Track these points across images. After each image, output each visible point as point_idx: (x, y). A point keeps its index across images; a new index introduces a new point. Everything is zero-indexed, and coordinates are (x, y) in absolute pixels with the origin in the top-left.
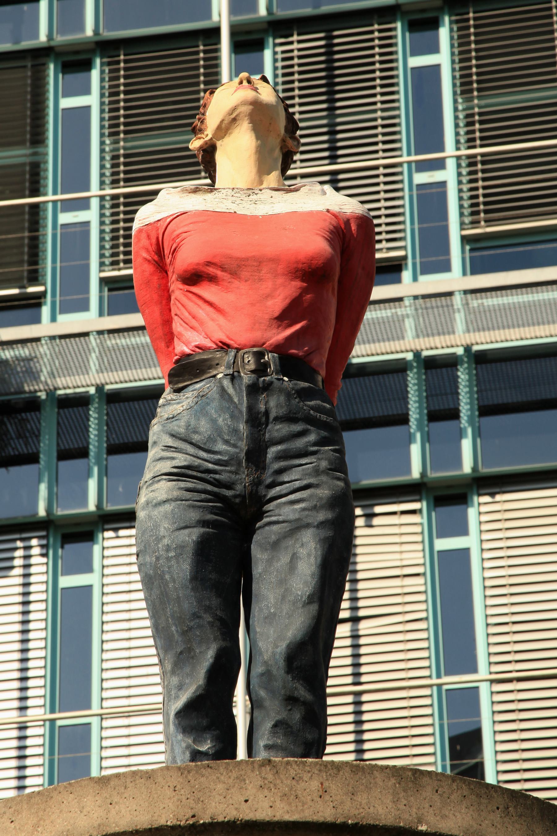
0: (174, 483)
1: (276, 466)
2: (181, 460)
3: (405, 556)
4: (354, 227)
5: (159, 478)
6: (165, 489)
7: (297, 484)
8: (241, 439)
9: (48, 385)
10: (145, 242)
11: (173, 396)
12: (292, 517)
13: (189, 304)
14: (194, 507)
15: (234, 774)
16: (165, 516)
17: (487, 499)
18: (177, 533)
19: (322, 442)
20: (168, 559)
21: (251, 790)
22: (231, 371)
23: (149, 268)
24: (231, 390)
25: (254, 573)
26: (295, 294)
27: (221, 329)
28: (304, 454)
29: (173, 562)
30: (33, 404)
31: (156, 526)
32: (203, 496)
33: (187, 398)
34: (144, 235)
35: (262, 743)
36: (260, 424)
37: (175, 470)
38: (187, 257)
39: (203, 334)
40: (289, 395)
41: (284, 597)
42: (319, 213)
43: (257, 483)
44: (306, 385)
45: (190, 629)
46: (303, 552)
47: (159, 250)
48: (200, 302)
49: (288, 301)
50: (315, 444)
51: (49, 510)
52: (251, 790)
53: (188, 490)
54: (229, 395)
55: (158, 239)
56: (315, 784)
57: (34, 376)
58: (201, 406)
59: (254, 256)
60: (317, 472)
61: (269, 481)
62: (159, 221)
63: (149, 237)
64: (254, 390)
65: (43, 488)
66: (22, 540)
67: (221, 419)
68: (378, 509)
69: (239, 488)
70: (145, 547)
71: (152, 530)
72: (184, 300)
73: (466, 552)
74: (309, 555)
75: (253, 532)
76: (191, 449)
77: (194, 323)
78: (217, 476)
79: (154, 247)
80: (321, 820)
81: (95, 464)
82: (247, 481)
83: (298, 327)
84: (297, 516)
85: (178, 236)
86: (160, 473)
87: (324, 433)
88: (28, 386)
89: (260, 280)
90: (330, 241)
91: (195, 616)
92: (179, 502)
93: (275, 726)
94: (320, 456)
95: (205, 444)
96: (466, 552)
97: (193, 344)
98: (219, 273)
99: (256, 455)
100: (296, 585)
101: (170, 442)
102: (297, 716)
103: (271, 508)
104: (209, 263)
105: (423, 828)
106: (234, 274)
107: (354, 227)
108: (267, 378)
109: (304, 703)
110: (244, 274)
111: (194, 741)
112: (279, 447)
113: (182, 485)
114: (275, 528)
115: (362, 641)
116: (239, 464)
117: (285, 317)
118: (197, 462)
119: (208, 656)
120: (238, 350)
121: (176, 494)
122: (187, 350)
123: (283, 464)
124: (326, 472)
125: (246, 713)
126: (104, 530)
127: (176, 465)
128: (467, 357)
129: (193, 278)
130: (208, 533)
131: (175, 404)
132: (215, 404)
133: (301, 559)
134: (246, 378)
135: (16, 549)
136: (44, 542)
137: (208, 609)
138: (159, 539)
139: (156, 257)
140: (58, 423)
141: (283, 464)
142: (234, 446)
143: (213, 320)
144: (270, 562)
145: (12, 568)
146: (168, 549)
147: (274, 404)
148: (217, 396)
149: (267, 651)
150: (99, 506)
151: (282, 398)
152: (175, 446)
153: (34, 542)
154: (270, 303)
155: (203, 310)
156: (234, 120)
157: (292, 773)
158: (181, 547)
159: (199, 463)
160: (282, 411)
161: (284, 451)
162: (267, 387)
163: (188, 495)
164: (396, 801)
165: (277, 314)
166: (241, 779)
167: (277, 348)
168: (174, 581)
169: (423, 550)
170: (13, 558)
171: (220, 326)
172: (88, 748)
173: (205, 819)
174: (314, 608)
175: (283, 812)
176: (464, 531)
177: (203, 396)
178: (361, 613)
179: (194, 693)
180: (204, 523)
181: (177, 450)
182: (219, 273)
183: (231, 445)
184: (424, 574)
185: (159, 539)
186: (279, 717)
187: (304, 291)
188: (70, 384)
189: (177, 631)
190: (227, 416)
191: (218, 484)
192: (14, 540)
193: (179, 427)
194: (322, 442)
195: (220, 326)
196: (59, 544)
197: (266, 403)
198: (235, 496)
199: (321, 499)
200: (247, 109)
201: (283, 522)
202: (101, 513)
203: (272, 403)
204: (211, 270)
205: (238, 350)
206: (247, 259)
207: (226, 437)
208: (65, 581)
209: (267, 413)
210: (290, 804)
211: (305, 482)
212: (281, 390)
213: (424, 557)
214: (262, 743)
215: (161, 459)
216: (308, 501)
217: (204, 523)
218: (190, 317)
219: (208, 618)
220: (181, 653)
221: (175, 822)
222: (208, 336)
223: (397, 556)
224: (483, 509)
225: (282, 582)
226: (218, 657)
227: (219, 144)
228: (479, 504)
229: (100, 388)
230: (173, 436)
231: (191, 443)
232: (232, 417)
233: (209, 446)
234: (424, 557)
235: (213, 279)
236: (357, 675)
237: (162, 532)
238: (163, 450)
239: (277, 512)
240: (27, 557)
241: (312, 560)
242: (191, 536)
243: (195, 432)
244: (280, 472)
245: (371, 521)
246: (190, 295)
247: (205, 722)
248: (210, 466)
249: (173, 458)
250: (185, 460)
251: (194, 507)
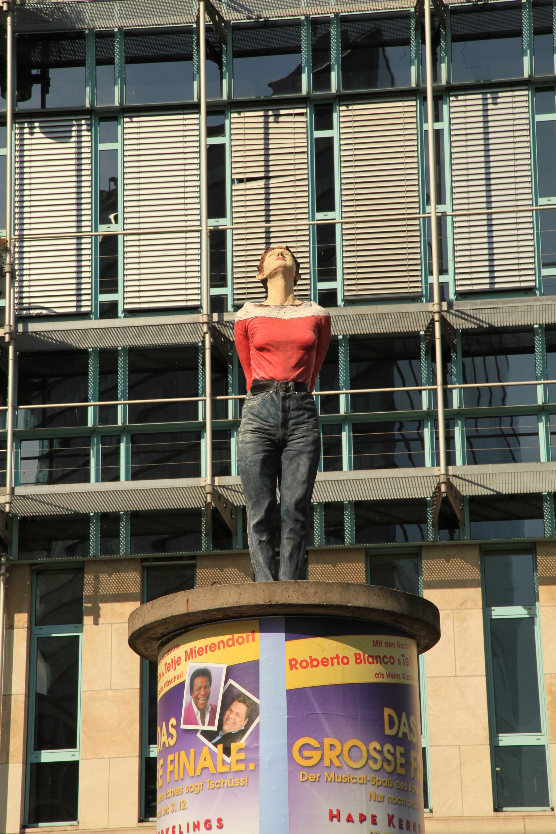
1: (292, 428)
2: (256, 425)
3: (297, 141)
4: (323, 321)
6: (249, 437)
7: (300, 435)
8: (279, 418)
9: (90, 26)
10: (240, 327)
11: (251, 397)
12: (297, 449)
14: (260, 445)
15: (284, 586)
16: (250, 448)
17: (344, 108)
19: (309, 418)
20: (251, 466)
21: (290, 592)
22: (275, 390)
23: (241, 338)
24: (275, 398)
25: (282, 468)
26: (301, 357)
28: (303, 423)
29: (252, 467)
30: (80, 35)
31: (246, 452)
32: (264, 440)
34: (240, 324)
35: (285, 536)
36: (286, 412)
38: (258, 339)
40: (298, 400)
41: (294, 480)
42: (310, 317)
43: (285, 434)
44: (305, 393)
45: (259, 493)
46: (302, 463)
47: (246, 331)
48: (263, 359)
49: (298, 359)
50: (308, 418)
51: (92, 104)
52: (290, 592)
56: (313, 590)
57: (82, 21)
58: (263, 403)
60: (308, 430)
61: (289, 434)
63: (242, 325)
64: (284, 398)
65: (88, 89)
66: (76, 120)
68: (282, 112)
69: (278, 436)
72: (257, 356)
73: (331, 139)
74: (304, 464)
75: (282, 452)
76: (259, 421)
77: (261, 367)
78: (269, 432)
79: (244, 329)
80: (315, 603)
81: (118, 77)
82: (281, 434)
83: (301, 370)
84: (300, 449)
85: (254, 328)
87: (311, 413)
88: (78, 25)
89: (287, 351)
90: (314, 331)
91: (261, 488)
93: (290, 530)
94: (309, 423)
96: (331, 139)
98: (271, 348)
99: (285, 424)
101: (251, 417)
102: (298, 526)
104: (267, 344)
105: (350, 605)
106: (277, 349)
107: (323, 321)
108: (290, 393)
109: (301, 522)
110: (281, 348)
111: (260, 536)
112: (294, 421)
113: (256, 435)
114: (291, 452)
115: (271, 191)
116: (278, 427)
117: (297, 366)
119: (266, 504)
120: (278, 381)
121: (254, 439)
122: (258, 378)
123: (295, 427)
124: (311, 430)
125: (207, 237)
126: (124, 117)
128: (336, 20)
129: (261, 349)
130: (265, 455)
132: (269, 403)
134: (282, 393)
135: (73, 125)
136: (89, 122)
137: (266, 485)
138: (247, 457)
139: (245, 334)
140: (96, 48)
141: (295, 427)
142: (276, 420)
143: (268, 367)
144: (289, 465)
145: (71, 137)
146: (250, 462)
147: (291, 403)
150: (121, 103)
151: (295, 401)
153: (83, 122)
154: (291, 361)
156: (276, 273)
157: (305, 586)
158: (256, 461)
160: (295, 407)
161: (295, 422)
162: (290, 397)
164: (340, 596)
165: (293, 365)
166: (287, 588)
167: (294, 380)
168: (253, 475)
169: (307, 138)
170: (71, 131)
171: (271, 371)
172: (116, 252)
173: (274, 602)
174: (306, 485)
175: (301, 600)
176: (330, 126)
178: (271, 174)
180: (265, 451)
181: (254, 421)
182: (271, 348)
183: (276, 418)
184: (307, 152)
185: (247, 457)
186: (291, 527)
187: (304, 354)
188: (102, 24)
190: (274, 408)
191: (270, 434)
192: (72, 120)
193: (255, 411)
194: (309, 418)
195: (271, 371)
196: (97, 122)
197: (289, 403)
198: (276, 439)
199: (309, 441)
200: (281, 269)
202: (122, 107)
203: (291, 403)
204: (268, 347)
205: (278, 381)
206: (282, 342)
208: (102, 147)
209: (289, 407)
210: (304, 598)
211: (303, 435)
212: (295, 398)
213: (307, 142)
214: (285, 536)
215: (248, 424)
217: (265, 451)
219: (266, 489)
221: (264, 603)
222: (266, 373)
223: (292, 141)
224: (342, 114)
225: (293, 474)
226: (269, 504)
227: (269, 280)
228: (340, 111)
229: (120, 29)
231: (259, 418)
232: (276, 409)
233: (266, 419)
234: (307, 142)
235: (268, 350)
236: (268, 216)
237: (248, 455)
240: (79, 131)
241: (305, 466)
242: (259, 457)
243: (261, 414)
244: (294, 430)
245: (278, 119)
247: (264, 529)
248: (267, 427)
249: (252, 424)
251: (260, 445)
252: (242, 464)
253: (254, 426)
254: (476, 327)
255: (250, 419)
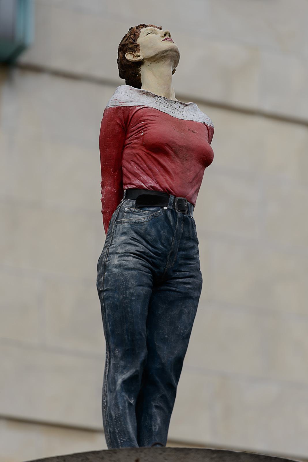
0: (137, 260)
2: (141, 248)
5: (129, 254)
12: (183, 291)
13: (149, 162)
16: (133, 276)
18: (137, 288)
27: (167, 182)
33: (145, 214)
34: (121, 111)
37: (137, 253)
39: (155, 180)
48: (156, 163)
53: (143, 265)
54: (169, 220)
55: (128, 116)
58: (154, 220)
59: (185, 146)
62: (131, 106)
67: (162, 232)
70: (115, 288)
71: (123, 282)
77: (151, 174)
78: (154, 260)
85: (144, 120)
86: (129, 252)
92: (139, 271)
95: (152, 242)
97: (150, 185)
100: (181, 327)
101: (135, 236)
103: (173, 283)
113: (141, 261)
118: (148, 251)
127: (139, 250)
131: (137, 214)
133: (184, 314)
138: (127, 288)
142: (165, 247)
143: (162, 175)
148: (163, 219)
149: (164, 358)
152: (138, 239)
155: (156, 167)
159: (148, 252)
163: (143, 268)
171: (167, 180)
177: (156, 216)
179: (134, 373)
185: (127, 288)
189: (128, 338)
201: (179, 292)
204: (167, 148)
207: (163, 242)
216: (192, 284)
218: (147, 169)
220: (128, 350)
222: (157, 182)
230: (136, 233)
235: (166, 154)
238: (131, 239)
239: (175, 286)
243: (149, 235)
246: (150, 157)
250: (143, 249)
252: (116, 295)
253: (137, 248)
254: (108, 182)
255: (134, 239)
